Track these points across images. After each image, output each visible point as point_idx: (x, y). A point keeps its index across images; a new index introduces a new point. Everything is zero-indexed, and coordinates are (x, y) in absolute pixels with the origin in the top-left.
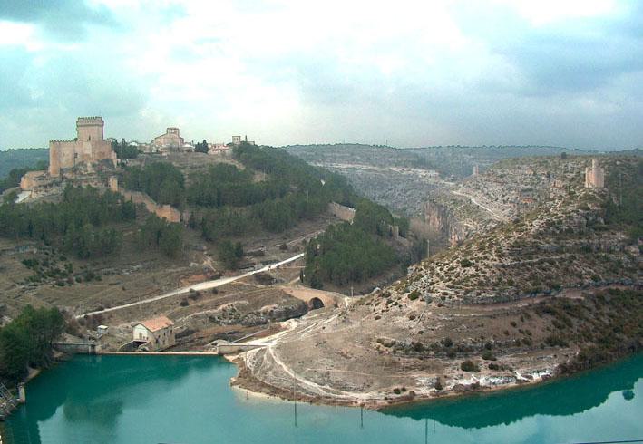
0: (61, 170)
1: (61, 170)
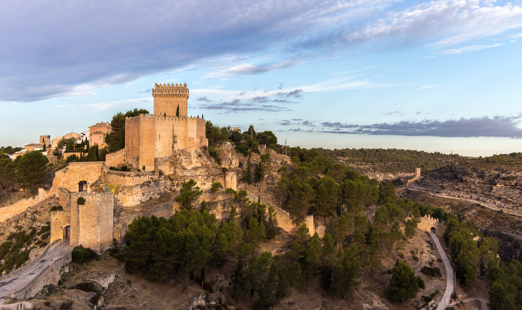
0: (156, 160)
1: (156, 160)
